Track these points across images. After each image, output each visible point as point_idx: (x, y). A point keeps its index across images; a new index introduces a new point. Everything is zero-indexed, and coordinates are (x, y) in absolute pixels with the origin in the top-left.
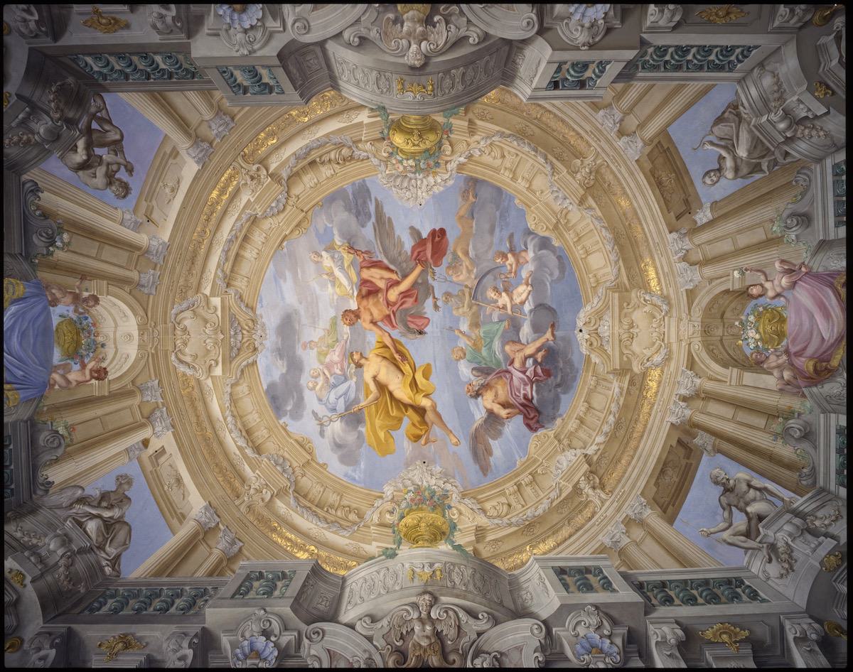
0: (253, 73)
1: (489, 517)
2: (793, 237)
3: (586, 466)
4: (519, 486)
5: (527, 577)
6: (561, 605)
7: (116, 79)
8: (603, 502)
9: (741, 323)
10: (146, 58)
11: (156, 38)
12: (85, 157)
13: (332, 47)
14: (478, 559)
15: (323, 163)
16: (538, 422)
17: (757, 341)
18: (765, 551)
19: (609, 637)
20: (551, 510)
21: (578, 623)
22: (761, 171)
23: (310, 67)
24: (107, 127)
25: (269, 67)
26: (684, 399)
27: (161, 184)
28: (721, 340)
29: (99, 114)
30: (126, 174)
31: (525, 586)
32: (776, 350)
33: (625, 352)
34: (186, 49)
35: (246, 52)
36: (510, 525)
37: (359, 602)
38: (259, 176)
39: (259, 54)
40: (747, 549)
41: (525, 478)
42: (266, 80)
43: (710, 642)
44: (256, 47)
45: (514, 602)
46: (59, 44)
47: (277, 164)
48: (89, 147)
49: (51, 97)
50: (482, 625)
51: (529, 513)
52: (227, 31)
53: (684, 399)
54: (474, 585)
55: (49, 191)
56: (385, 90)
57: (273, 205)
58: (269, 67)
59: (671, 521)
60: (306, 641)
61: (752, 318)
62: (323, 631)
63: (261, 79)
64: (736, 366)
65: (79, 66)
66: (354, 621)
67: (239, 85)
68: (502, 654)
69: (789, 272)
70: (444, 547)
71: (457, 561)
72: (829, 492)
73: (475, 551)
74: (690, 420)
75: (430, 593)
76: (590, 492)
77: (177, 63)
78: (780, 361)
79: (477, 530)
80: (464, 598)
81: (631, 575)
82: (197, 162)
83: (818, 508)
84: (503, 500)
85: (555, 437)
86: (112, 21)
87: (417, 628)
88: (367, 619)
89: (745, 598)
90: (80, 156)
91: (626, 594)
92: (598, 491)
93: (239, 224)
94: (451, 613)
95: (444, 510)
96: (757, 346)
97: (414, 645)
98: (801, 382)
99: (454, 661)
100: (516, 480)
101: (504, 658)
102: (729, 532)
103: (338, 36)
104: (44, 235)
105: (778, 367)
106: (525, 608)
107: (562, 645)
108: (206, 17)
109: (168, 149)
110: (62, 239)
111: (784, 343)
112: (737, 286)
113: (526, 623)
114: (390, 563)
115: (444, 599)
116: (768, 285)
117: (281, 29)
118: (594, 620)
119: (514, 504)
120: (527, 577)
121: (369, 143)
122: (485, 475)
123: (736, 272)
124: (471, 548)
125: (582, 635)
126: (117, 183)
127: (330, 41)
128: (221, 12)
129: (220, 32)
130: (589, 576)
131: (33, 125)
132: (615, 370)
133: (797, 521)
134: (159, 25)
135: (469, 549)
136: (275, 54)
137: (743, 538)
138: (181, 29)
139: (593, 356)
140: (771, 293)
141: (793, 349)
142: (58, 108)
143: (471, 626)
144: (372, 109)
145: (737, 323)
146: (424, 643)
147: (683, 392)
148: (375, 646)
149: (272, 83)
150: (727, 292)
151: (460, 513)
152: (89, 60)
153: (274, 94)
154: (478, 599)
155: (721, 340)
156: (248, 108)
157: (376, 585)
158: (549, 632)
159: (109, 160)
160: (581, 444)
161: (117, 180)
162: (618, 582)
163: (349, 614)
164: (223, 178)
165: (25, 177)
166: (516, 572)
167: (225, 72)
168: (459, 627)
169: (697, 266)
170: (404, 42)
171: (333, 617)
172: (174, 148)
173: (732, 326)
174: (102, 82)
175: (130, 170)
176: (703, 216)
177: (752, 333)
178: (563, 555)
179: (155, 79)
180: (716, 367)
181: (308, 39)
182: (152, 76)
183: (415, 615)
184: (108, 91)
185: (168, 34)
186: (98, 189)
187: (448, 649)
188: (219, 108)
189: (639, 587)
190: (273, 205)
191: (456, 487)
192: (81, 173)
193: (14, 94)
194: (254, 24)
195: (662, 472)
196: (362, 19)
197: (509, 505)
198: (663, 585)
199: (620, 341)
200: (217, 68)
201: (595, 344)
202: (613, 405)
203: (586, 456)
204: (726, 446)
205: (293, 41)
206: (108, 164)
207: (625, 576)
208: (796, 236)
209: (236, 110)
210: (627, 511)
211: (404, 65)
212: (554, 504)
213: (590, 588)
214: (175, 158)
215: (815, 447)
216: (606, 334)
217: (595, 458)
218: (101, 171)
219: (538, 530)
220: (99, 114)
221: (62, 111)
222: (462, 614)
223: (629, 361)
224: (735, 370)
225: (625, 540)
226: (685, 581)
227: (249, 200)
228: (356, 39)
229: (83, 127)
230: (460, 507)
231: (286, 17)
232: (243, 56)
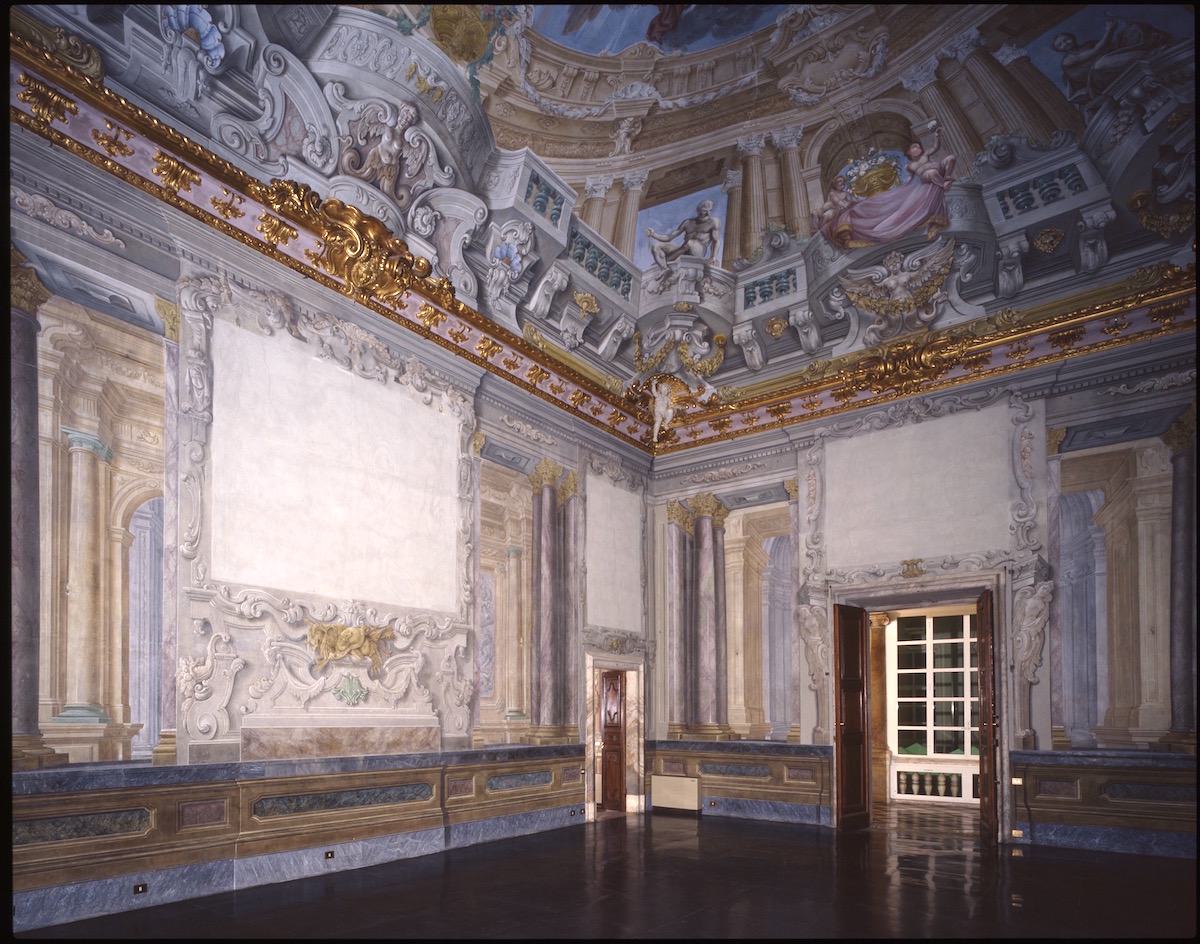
1: (527, 79)
2: (984, 159)
3: (645, 112)
4: (580, 74)
5: (507, 162)
6: (513, 208)
8: (622, 152)
9: (873, 153)
14: (483, 111)
16: (663, 33)
17: (857, 174)
18: (663, 272)
19: (523, 256)
20: (579, 122)
21: (512, 231)
22: (1074, 90)
26: (769, 142)
28: (849, 143)
31: (500, 169)
32: (852, 195)
33: (799, 61)
36: (536, 103)
37: (340, 58)
40: (657, 262)
41: (592, 72)
43: (575, 302)
45: (482, 175)
50: (443, 178)
51: (562, 107)
53: (769, 142)
54: (461, 135)
59: (643, 206)
60: (262, 63)
61: (881, 160)
62: (287, 65)
64: (822, 168)
66: (327, 79)
68: (442, 217)
69: (942, 172)
70: (463, 70)
71: (464, 96)
72: (736, 283)
73: (487, 100)
74: (749, 157)
75: (418, 110)
76: (623, 136)
78: (841, 203)
79: (505, 82)
80: (444, 140)
81: (577, 222)
83: (719, 281)
84: (554, 73)
85: (657, 63)
87: (386, 138)
88: (340, 87)
89: (620, 290)
91: (560, 235)
92: (628, 141)
94: (424, 146)
95: (494, 29)
96: (851, 177)
97: (374, 154)
98: (825, 227)
99: (402, 197)
100: (582, 66)
101: (442, 222)
102: (662, 244)
105: (835, 204)
106: (485, 189)
107: (488, 240)
111: (861, 198)
112: (917, 131)
113: (477, 202)
114: (397, 36)
115: (426, 126)
116: (924, 159)
118: (523, 237)
119: (558, 86)
120: (507, 162)
122: (564, 33)
123: (934, 123)
124: (485, 94)
125: (507, 241)
130: (551, 200)
132: (772, 64)
133: (701, 274)
135: (484, 94)
137: (663, 254)
139: (777, 32)
140: (914, 166)
141: (856, 208)
143: (435, 174)
145: (872, 149)
146: (385, 159)
147: (776, 137)
148: (337, 128)
150: (908, 124)
151: (507, 49)
154: (455, 151)
155: (849, 143)
157: (369, 52)
158: (486, 223)
160: (666, 90)
162: (564, 221)
163: (323, 65)
164: (723, 470)
166: (503, 150)
168: (423, 166)
169: (935, 79)
171: (304, 57)
173: (868, 146)
176: (1006, 56)
177: (864, 167)
178: (549, 167)
180: (816, 152)
183: (391, 123)
187: (403, 182)
189: (573, 235)
191: (528, 16)
195: (683, 169)
197: (554, 84)
198: (588, 245)
199: (810, 49)
201: (796, 24)
202: (728, 87)
203: (656, 103)
204: (738, 197)
207: (573, 219)
208: (986, 162)
210: (627, 175)
212: (588, 119)
213: (542, 209)
215: (769, 260)
216: (812, 29)
217: (659, 113)
219: (553, 130)
222: (432, 155)
223: (787, 72)
224: (819, 170)
225: (601, 194)
226: (602, 253)
230: (512, 42)
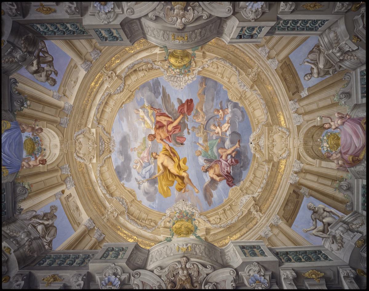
0: (110, 32)
1: (212, 224)
2: (343, 103)
3: (253, 202)
4: (224, 210)
5: (228, 250)
6: (243, 262)
7: (50, 34)
8: (261, 217)
9: (321, 140)
10: (63, 25)
11: (67, 17)
12: (37, 68)
13: (143, 20)
14: (207, 242)
15: (140, 71)
16: (233, 183)
17: (327, 148)
18: (331, 239)
19: (264, 276)
20: (238, 221)
21: (250, 270)
22: (329, 74)
23: (134, 29)
24: (46, 55)
25: (116, 29)
26: (296, 173)
27: (70, 80)
28: (312, 147)
29: (43, 49)
30: (55, 75)
31: (227, 254)
32: (336, 152)
33: (271, 152)
34: (80, 21)
35: (106, 23)
36: (221, 227)
37: (155, 261)
38: (112, 76)
39: (112, 23)
40: (323, 238)
41: (227, 207)
42: (115, 34)
43: (307, 278)
44: (111, 20)
45: (223, 261)
46: (25, 19)
47: (120, 71)
48: (38, 64)
49: (22, 42)
50: (209, 271)
51: (229, 222)
52: (98, 13)
53: (296, 173)
54: (205, 254)
55: (21, 83)
56: (166, 39)
57: (118, 89)
58: (116, 29)
59: (290, 225)
60: (132, 278)
61: (325, 138)
62: (140, 273)
63: (113, 34)
64: (318, 159)
65: (34, 28)
66: (153, 269)
67: (103, 37)
68: (217, 283)
69: (341, 118)
70: (192, 237)
71: (198, 243)
72: (359, 213)
73: (206, 239)
74: (298, 182)
75: (186, 257)
76: (255, 213)
77: (77, 27)
78: (338, 156)
79: (206, 230)
80: (201, 259)
81: (273, 249)
82: (85, 70)
83: (354, 220)
84: (218, 216)
85: (240, 189)
86: (49, 9)
87: (180, 272)
88: (159, 268)
89: (322, 259)
90: (35, 68)
91: (271, 257)
92: (259, 213)
93: (103, 97)
94: (195, 265)
95: (192, 221)
96: (328, 150)
97: (179, 279)
98: (346, 165)
99: (197, 286)
100: (223, 208)
101: (218, 285)
102: (315, 230)
103: (146, 15)
104: (19, 102)
105: (337, 159)
106: (227, 263)
107: (243, 280)
108: (89, 7)
109: (73, 65)
110: (27, 104)
111: (339, 149)
112: (319, 124)
113: (227, 270)
114: (169, 244)
115: (192, 259)
116: (332, 123)
117: (122, 13)
118: (257, 269)
119: (222, 218)
120: (228, 250)
121: (159, 62)
122: (210, 206)
123: (318, 118)
124: (204, 237)
125: (252, 275)
126: (51, 79)
127: (143, 18)
128: (96, 5)
129: (95, 14)
130: (255, 250)
131: (14, 54)
132: (266, 160)
133: (345, 226)
134: (69, 11)
135: (203, 238)
136: (119, 23)
137: (321, 233)
138: (78, 13)
139: (256, 154)
140: (333, 127)
141: (343, 151)
142: (25, 47)
143: (204, 271)
144: (161, 47)
145: (319, 140)
146: (184, 278)
147: (295, 170)
148: (162, 280)
149: (118, 36)
150: (314, 126)
151: (199, 222)
152: (39, 26)
153: (118, 41)
154: (207, 259)
155: (312, 147)
156: (107, 47)
157: (163, 253)
158: (237, 274)
159: (47, 69)
160: (251, 192)
161: (51, 78)
162: (267, 252)
163: (151, 266)
164: (97, 77)
165: (11, 77)
166: (223, 248)
167: (97, 31)
168: (199, 272)
169: (302, 115)
170: (175, 18)
171: (144, 267)
172: (75, 64)
173: (317, 141)
174: (44, 36)
175: (56, 74)
176: (304, 94)
177: (325, 144)
178: (243, 240)
179: (67, 34)
180: (310, 159)
181: (133, 17)
182: (66, 33)
183: (180, 266)
184: (47, 39)
185: (73, 15)
186: (42, 82)
187: (194, 281)
188: (95, 47)
189: (277, 254)
190: (118, 89)
191: (197, 211)
192: (35, 75)
193: (6, 41)
194: (110, 10)
195: (287, 204)
196: (157, 8)
197: (220, 219)
198: (287, 253)
199: (268, 148)
200: (94, 29)
201: (257, 149)
202: (265, 175)
203: (253, 197)
204: (314, 193)
205: (127, 18)
206: (47, 71)
207: (270, 250)
208: (344, 102)
209: (102, 48)
210: (271, 221)
211: (175, 28)
212: (240, 218)
213: (255, 255)
214: (75, 68)
215: (353, 194)
216: (262, 145)
217: (257, 198)
218: (44, 74)
219: (233, 230)
220: (43, 49)
221: (27, 48)
222: (200, 266)
223: (272, 156)
224: (318, 160)
225: (271, 234)
226: (296, 252)
227: (108, 87)
228: (154, 17)
229: (36, 55)
230: (199, 220)
231: (124, 7)
232: (105, 24)
